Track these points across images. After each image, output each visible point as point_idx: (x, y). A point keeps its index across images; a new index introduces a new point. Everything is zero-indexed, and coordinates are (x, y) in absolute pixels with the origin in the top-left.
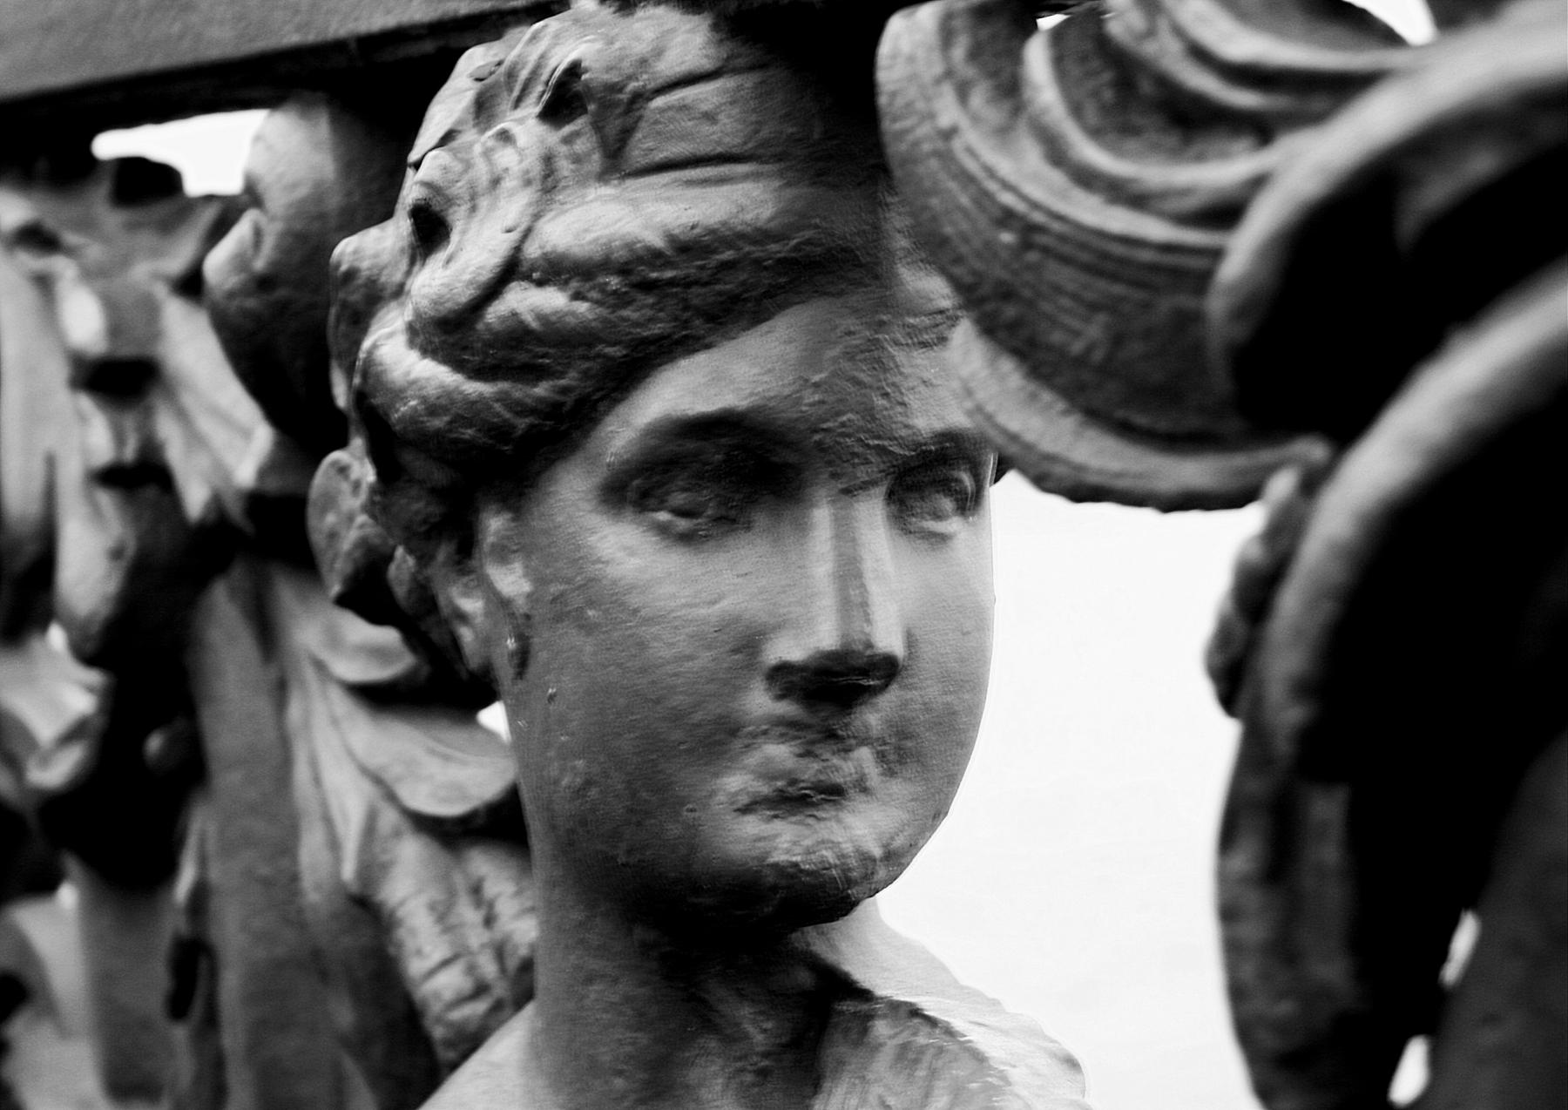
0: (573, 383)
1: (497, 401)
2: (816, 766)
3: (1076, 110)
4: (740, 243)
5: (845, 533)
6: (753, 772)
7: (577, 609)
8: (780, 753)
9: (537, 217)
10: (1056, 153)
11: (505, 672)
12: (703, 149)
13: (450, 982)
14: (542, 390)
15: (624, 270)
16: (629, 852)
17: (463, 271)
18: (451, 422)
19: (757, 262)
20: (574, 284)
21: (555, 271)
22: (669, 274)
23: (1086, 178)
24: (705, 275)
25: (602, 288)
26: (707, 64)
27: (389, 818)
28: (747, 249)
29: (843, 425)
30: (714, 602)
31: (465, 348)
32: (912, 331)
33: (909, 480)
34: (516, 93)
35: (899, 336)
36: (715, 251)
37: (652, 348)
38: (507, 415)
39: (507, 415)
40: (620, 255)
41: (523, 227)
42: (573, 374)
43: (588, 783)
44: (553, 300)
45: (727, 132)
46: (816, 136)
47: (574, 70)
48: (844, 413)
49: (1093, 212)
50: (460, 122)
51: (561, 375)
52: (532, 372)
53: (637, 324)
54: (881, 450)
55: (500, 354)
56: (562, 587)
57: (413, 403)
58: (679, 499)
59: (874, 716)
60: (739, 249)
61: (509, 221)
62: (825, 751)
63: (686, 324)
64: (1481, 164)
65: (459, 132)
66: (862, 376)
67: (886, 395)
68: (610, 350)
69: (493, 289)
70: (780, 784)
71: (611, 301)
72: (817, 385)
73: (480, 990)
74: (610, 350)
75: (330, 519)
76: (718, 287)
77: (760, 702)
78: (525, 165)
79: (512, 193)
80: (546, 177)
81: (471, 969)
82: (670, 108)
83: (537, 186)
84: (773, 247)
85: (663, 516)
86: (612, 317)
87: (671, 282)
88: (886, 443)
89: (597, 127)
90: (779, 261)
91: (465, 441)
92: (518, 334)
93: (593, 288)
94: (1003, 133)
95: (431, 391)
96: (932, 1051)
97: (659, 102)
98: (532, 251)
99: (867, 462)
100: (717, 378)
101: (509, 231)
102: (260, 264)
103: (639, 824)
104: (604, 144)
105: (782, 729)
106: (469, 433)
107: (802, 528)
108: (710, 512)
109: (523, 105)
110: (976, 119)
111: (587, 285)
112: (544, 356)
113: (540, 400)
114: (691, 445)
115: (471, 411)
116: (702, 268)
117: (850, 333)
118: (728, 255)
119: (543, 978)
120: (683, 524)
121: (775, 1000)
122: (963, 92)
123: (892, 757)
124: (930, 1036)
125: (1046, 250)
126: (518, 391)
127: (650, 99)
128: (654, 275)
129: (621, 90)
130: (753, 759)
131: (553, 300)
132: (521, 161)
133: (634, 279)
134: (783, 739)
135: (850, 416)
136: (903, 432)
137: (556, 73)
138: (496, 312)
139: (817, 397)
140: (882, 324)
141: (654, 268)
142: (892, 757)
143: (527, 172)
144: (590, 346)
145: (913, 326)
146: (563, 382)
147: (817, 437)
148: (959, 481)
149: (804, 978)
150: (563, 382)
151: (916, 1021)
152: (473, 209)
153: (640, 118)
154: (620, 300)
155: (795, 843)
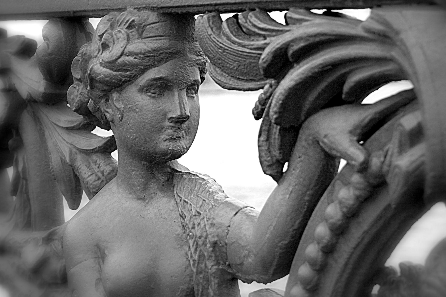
0: (134, 72)
1: (119, 75)
2: (176, 133)
3: (232, 32)
4: (164, 50)
5: (180, 97)
6: (166, 135)
7: (134, 109)
8: (170, 131)
9: (127, 45)
10: (229, 39)
11: (117, 121)
12: (156, 35)
13: (93, 178)
14: (128, 73)
15: (144, 54)
16: (144, 149)
17: (113, 54)
18: (110, 79)
19: (166, 53)
20: (135, 56)
21: (131, 54)
22: (151, 55)
23: (234, 42)
24: (158, 55)
25: (140, 57)
26: (157, 21)
27: (74, 150)
28: (165, 51)
29: (180, 79)
30: (159, 108)
31: (113, 66)
32: (190, 64)
33: (189, 88)
34: (119, 24)
35: (188, 65)
36: (159, 51)
37: (148, 67)
38: (121, 78)
39: (121, 78)
40: (143, 52)
41: (124, 47)
42: (134, 71)
43: (136, 137)
44: (131, 59)
45: (159, 32)
46: (175, 32)
47: (133, 21)
48: (180, 77)
49: (236, 47)
50: (108, 28)
51: (132, 71)
52: (127, 70)
53: (146, 63)
54: (186, 83)
55: (120, 67)
56: (131, 106)
57: (102, 76)
58: (152, 91)
59: (184, 125)
60: (163, 51)
61: (122, 45)
62: (178, 131)
63: (154, 63)
64: (302, 44)
65: (108, 30)
66: (182, 71)
67: (186, 74)
68: (141, 67)
69: (120, 57)
70: (171, 136)
71: (141, 59)
72: (176, 73)
73: (99, 179)
74: (141, 67)
75: (72, 96)
76: (160, 57)
77: (167, 123)
78: (124, 36)
79: (122, 41)
80: (128, 38)
81: (96, 175)
82: (150, 28)
83: (126, 40)
84: (169, 50)
85: (150, 94)
86: (142, 62)
87: (152, 56)
88: (186, 82)
89: (137, 30)
90: (170, 53)
91: (113, 82)
92: (124, 64)
93: (138, 57)
94: (219, 35)
95: (106, 74)
96: (195, 179)
97: (148, 26)
98: (126, 51)
99: (183, 85)
100: (159, 72)
101: (122, 47)
102: (49, 51)
103: (146, 144)
104: (138, 33)
105: (171, 128)
106: (113, 81)
107: (173, 96)
108: (158, 93)
109: (120, 26)
110: (214, 33)
111: (137, 56)
112: (129, 68)
113: (127, 75)
114: (155, 82)
115: (114, 77)
116: (157, 54)
117: (180, 64)
118: (161, 52)
119: (120, 172)
120: (153, 95)
121: (165, 173)
122: (212, 29)
123: (187, 132)
124: (194, 177)
125: (227, 53)
126: (123, 74)
127: (147, 26)
128: (149, 55)
129: (142, 24)
130: (166, 133)
131: (131, 59)
132: (123, 36)
133: (146, 55)
134: (171, 129)
135: (181, 77)
136: (189, 80)
137: (80, 13)
138: (120, 61)
139: (176, 74)
140: (185, 63)
141: (149, 53)
142: (187, 132)
143: (125, 38)
144: (137, 66)
145: (190, 63)
146: (132, 72)
147: (176, 81)
148: (196, 88)
149: (169, 170)
150: (132, 72)
151: (191, 175)
152: (114, 43)
153: (145, 29)
154: (143, 59)
155: (173, 146)
